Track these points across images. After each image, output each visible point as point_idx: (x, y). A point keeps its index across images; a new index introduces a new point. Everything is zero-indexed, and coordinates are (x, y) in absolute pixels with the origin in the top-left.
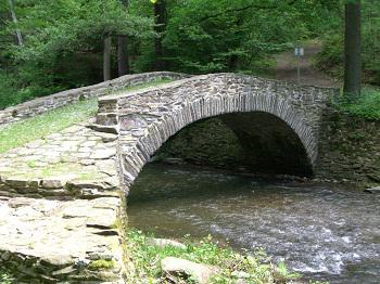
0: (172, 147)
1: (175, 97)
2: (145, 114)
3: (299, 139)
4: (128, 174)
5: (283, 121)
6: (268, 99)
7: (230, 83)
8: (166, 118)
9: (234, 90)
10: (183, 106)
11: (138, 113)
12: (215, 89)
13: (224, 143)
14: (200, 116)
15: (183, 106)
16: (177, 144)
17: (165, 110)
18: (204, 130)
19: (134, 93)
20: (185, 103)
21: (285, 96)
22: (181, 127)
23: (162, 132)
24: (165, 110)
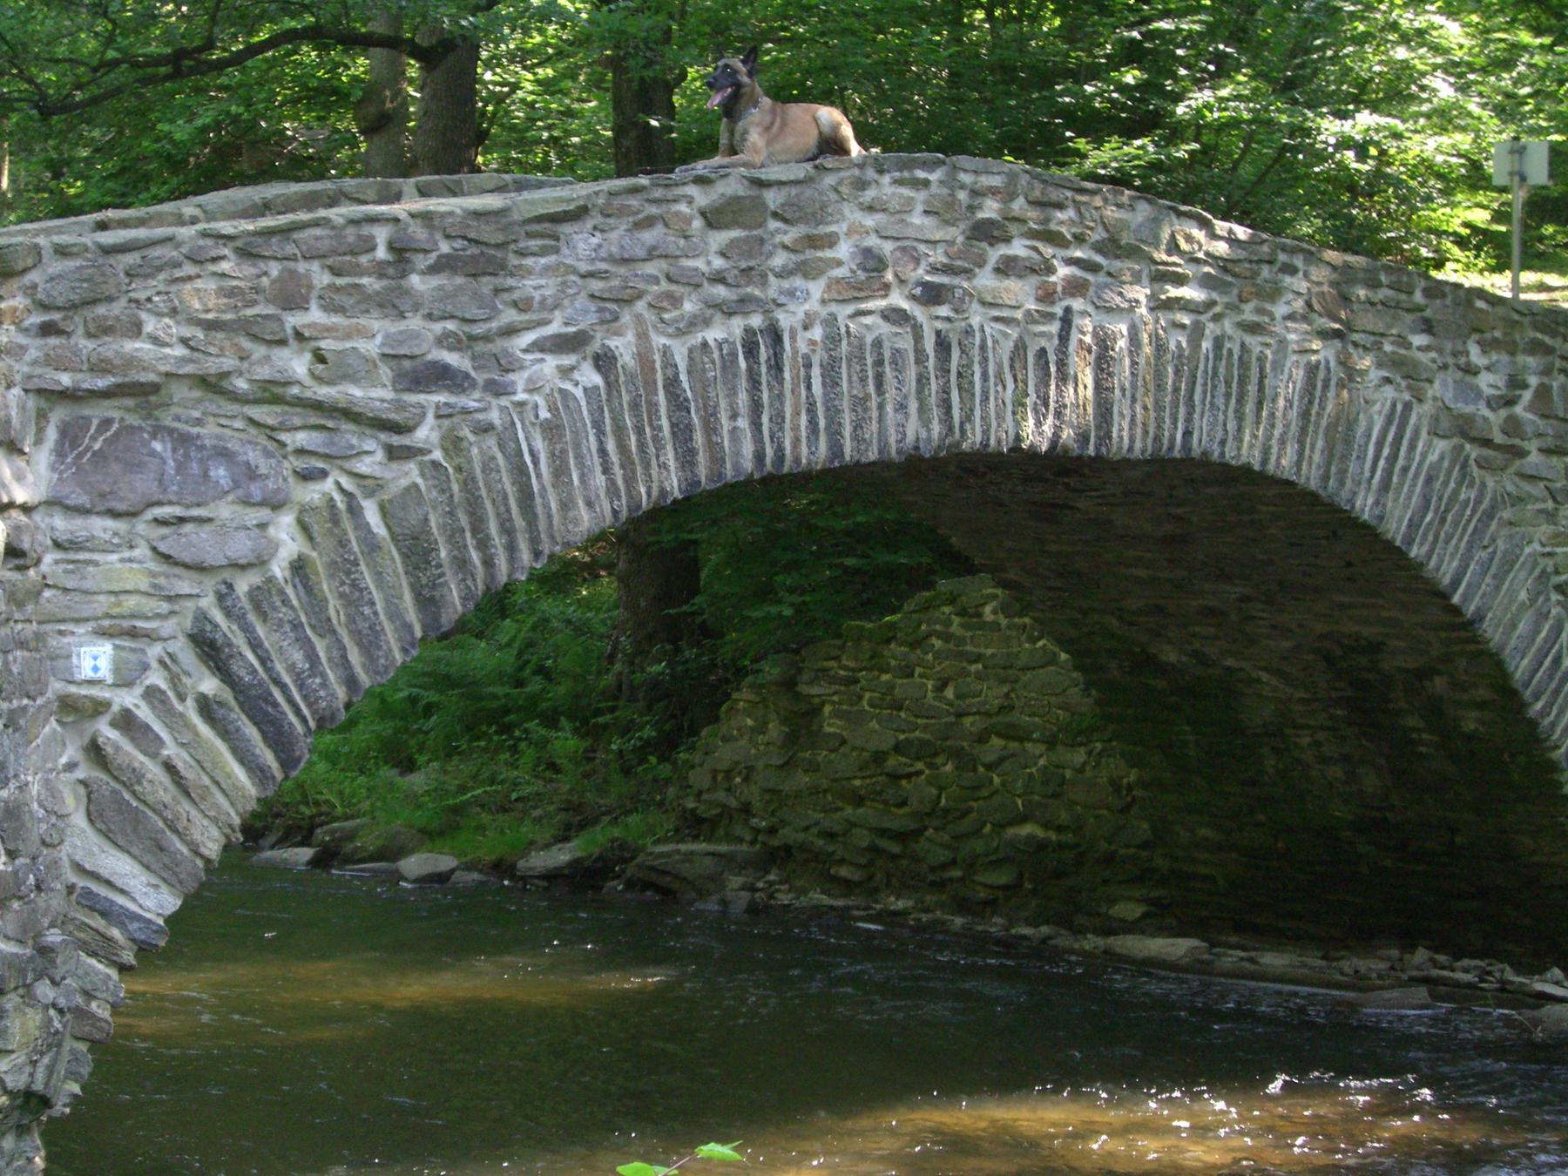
0: (699, 778)
1: (536, 284)
2: (272, 392)
3: (1508, 697)
4: (119, 865)
5: (1394, 555)
6: (1288, 385)
7: (988, 233)
8: (453, 444)
9: (1020, 293)
10: (605, 362)
11: (212, 385)
12: (872, 262)
13: (1013, 733)
14: (742, 457)
15: (605, 362)
16: (725, 755)
17: (441, 376)
18: (895, 652)
19: (506, 479)
20: (623, 346)
21: (1404, 370)
22: (585, 521)
23: (417, 551)
24: (441, 376)
